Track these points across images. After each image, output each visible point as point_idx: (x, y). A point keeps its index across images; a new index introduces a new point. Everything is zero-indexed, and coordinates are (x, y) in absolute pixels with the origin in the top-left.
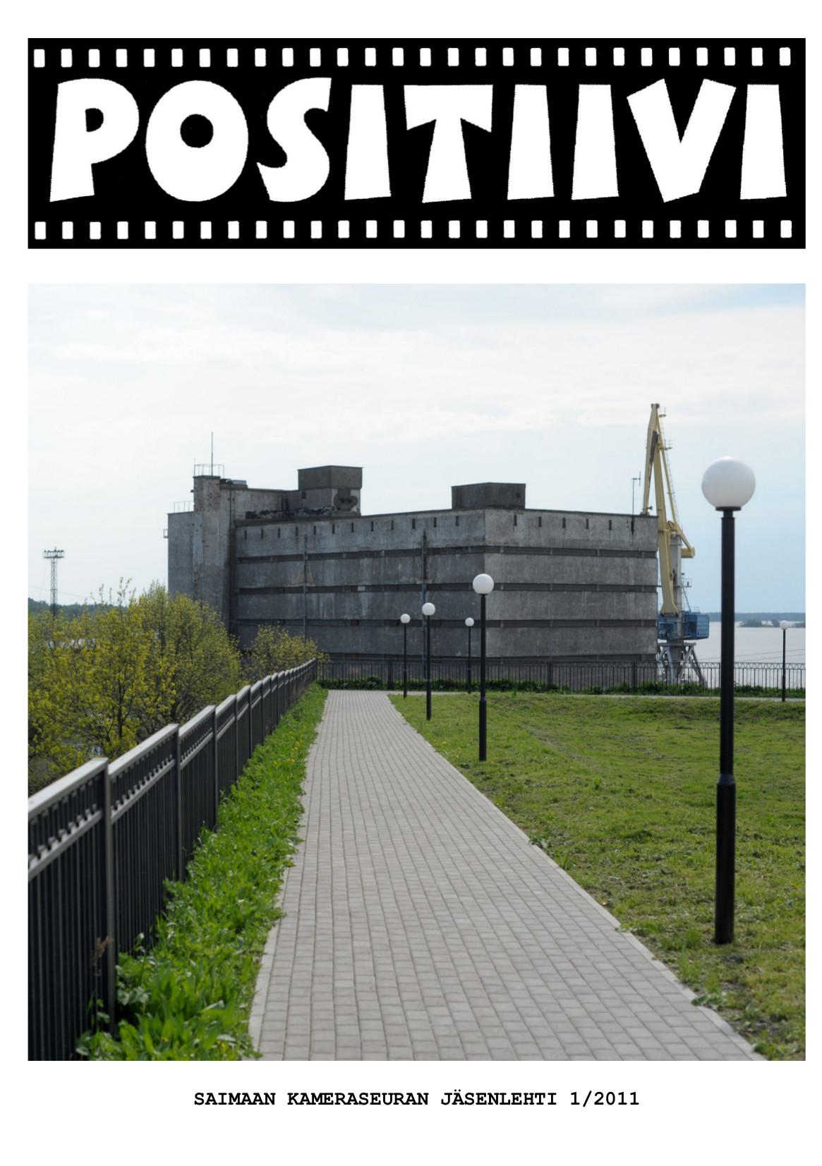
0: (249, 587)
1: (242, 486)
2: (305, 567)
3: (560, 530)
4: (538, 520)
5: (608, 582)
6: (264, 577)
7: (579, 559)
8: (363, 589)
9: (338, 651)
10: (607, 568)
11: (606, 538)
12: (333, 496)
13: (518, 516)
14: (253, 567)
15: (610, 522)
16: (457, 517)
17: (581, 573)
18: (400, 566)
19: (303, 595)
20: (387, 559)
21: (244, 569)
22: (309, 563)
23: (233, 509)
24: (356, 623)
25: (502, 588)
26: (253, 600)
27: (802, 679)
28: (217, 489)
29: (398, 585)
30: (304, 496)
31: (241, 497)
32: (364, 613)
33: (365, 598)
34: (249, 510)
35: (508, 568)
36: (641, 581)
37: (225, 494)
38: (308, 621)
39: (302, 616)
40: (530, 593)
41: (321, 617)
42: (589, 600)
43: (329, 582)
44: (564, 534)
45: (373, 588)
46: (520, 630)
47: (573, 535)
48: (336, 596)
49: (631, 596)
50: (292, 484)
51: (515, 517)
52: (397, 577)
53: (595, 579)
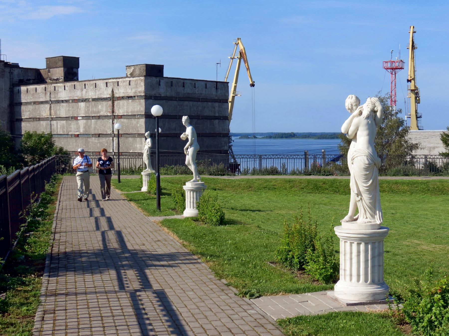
1: (16, 66)
3: (182, 88)
5: (205, 114)
6: (29, 113)
7: (191, 103)
13: (161, 80)
18: (100, 106)
22: (52, 105)
24: (78, 136)
31: (16, 72)
32: (82, 131)
33: (82, 123)
37: (7, 70)
40: (167, 119)
44: (184, 90)
45: (87, 118)
47: (188, 90)
48: (66, 122)
52: (99, 112)
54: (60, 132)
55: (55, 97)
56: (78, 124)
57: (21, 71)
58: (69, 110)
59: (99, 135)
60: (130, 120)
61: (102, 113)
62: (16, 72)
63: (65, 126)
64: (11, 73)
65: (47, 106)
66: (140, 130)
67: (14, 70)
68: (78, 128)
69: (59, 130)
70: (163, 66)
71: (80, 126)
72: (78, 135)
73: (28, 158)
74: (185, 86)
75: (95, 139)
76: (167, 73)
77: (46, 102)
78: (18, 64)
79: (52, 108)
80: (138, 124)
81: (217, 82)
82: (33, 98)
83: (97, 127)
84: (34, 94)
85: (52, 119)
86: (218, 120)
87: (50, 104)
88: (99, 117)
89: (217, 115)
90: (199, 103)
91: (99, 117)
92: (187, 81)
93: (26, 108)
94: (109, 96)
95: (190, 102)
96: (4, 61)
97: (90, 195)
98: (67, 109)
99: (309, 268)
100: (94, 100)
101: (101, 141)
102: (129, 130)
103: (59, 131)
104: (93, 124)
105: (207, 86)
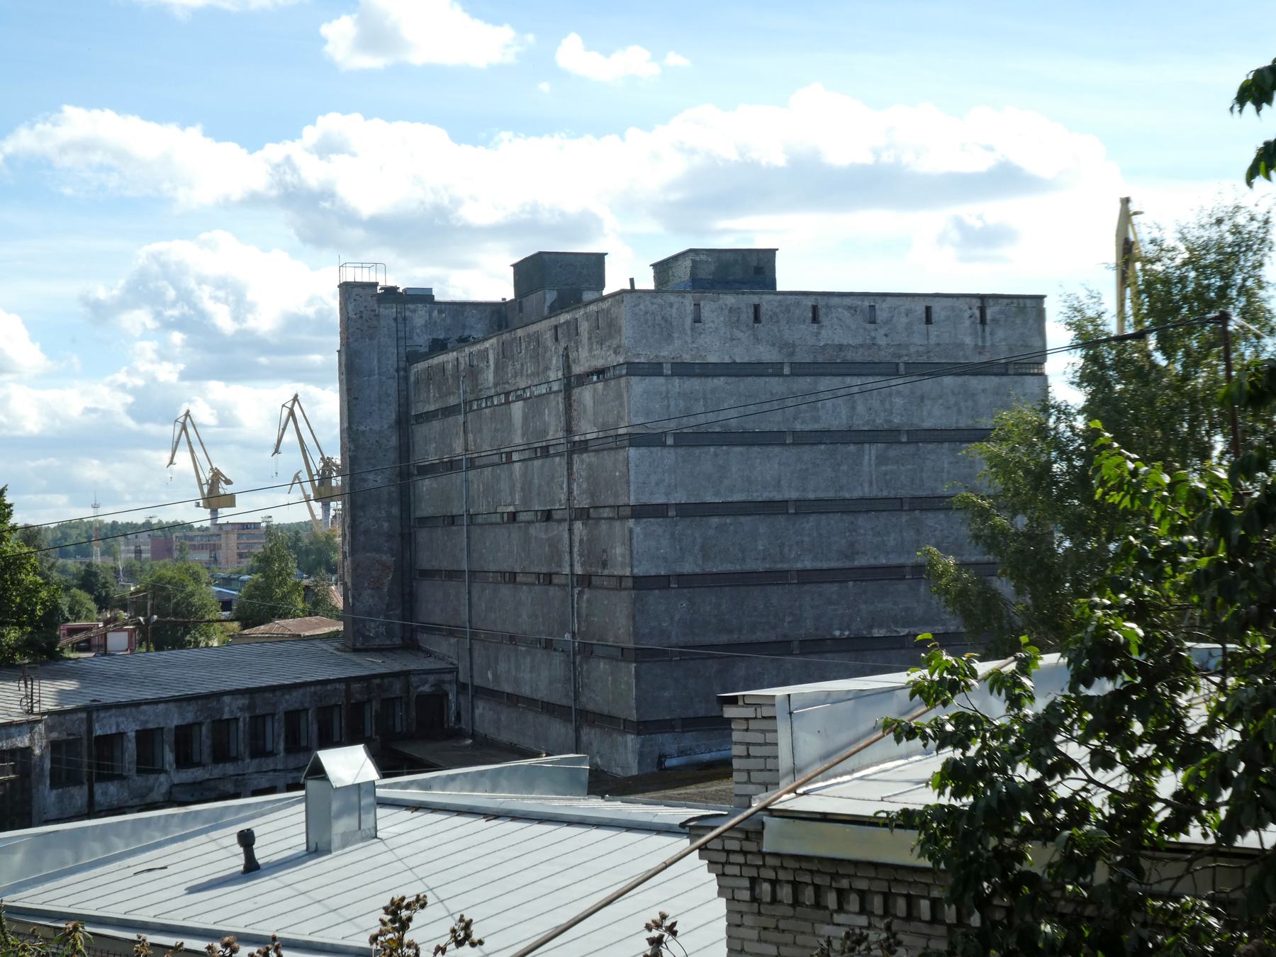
1: (423, 297)
5: (927, 424)
12: (548, 303)
13: (702, 303)
17: (861, 408)
25: (670, 441)
27: (347, 841)
34: (435, 336)
35: (682, 403)
36: (632, 297)
37: (389, 311)
42: (882, 460)
44: (818, 334)
46: (715, 521)
47: (834, 333)
51: (697, 305)
53: (897, 420)
57: (440, 312)
62: (419, 316)
67: (414, 311)
74: (825, 321)
76: (787, 279)
78: (431, 290)
81: (982, 298)
92: (836, 300)
97: (996, 902)
105: (935, 317)
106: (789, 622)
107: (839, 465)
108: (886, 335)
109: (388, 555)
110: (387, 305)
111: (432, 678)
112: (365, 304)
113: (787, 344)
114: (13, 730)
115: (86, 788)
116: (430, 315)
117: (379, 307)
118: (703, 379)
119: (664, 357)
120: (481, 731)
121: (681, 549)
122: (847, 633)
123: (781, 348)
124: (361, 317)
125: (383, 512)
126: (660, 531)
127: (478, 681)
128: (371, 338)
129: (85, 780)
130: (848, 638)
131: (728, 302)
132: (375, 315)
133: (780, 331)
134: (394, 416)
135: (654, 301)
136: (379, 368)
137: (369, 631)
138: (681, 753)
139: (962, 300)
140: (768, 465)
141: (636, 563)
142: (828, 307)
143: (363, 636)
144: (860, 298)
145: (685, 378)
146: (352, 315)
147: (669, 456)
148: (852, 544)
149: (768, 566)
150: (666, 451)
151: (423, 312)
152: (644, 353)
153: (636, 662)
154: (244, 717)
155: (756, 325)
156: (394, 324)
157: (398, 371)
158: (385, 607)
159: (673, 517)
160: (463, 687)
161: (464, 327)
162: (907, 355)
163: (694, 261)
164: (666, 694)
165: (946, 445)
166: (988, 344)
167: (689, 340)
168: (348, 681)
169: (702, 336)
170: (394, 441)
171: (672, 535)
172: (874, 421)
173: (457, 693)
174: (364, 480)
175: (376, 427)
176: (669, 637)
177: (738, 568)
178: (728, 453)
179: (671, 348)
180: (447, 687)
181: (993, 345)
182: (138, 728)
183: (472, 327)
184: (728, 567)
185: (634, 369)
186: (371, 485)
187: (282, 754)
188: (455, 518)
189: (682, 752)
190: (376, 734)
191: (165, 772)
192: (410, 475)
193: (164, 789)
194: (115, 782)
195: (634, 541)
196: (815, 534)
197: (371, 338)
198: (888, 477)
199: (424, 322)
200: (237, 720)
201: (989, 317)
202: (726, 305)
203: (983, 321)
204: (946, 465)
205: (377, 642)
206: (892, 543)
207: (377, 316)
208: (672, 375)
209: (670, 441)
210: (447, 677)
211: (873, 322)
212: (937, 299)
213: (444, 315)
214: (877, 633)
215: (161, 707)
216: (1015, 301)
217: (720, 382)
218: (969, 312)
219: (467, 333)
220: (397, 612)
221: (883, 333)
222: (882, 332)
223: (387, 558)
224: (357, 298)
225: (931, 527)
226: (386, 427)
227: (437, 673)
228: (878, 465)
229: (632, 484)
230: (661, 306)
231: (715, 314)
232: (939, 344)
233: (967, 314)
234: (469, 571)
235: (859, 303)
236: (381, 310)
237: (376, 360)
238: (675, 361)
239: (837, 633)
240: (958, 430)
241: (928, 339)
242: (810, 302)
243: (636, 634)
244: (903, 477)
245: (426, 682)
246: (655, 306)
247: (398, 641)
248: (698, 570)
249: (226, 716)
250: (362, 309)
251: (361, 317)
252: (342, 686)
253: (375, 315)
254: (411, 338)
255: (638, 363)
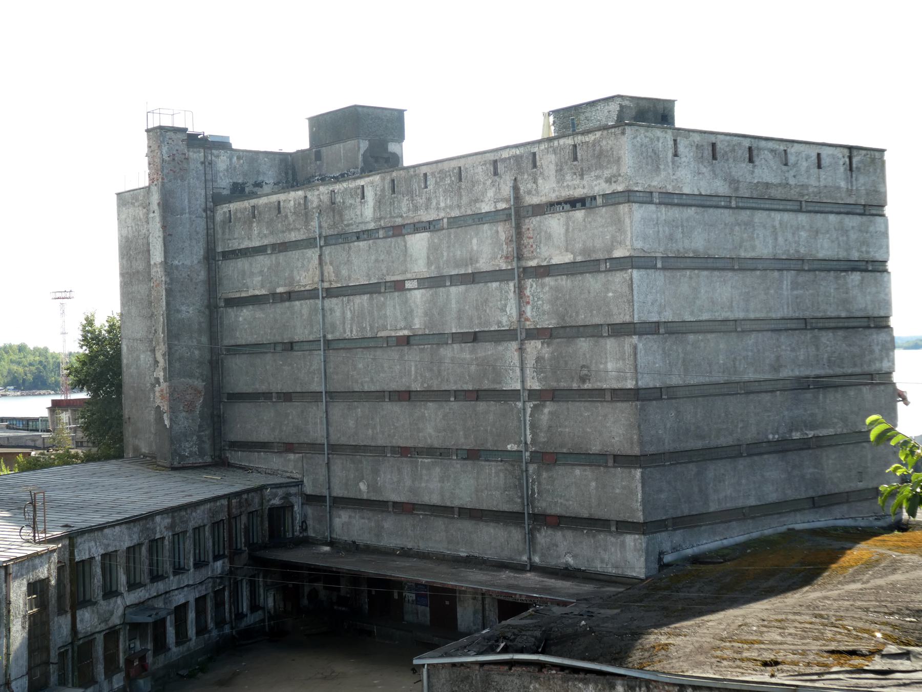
0: (238, 295)
1: (223, 145)
2: (320, 256)
3: (745, 166)
4: (710, 148)
5: (821, 255)
6: (260, 278)
8: (415, 284)
9: (378, 389)
10: (817, 232)
11: (813, 182)
12: (362, 151)
13: (679, 139)
14: (242, 264)
15: (819, 155)
16: (575, 146)
18: (475, 241)
19: (319, 302)
20: (452, 231)
21: (232, 269)
22: (327, 250)
23: (209, 177)
24: (406, 341)
26: (245, 314)
28: (183, 147)
29: (473, 274)
30: (318, 156)
32: (418, 324)
33: (418, 297)
35: (667, 229)
36: (868, 252)
37: (197, 156)
38: (328, 343)
39: (317, 334)
41: (348, 335)
43: (360, 279)
44: (753, 172)
45: (433, 282)
48: (371, 299)
49: (856, 277)
50: (303, 143)
52: (472, 260)
54: (351, 331)
55: (334, 225)
56: (406, 302)
57: (239, 158)
58: (377, 261)
59: (475, 337)
60: (579, 277)
61: (484, 265)
62: (222, 162)
63: (366, 311)
64: (208, 164)
65: (312, 255)
66: (615, 311)
67: (218, 156)
68: (409, 315)
69: (348, 327)
70: (672, 102)
71: (412, 311)
72: (408, 337)
73: (20, 458)
75: (462, 350)
76: (681, 121)
77: (309, 243)
79: (327, 258)
80: (608, 290)
82: (272, 233)
83: (467, 307)
84: (272, 220)
85: (330, 293)
86: (859, 273)
87: (321, 247)
88: (473, 278)
89: (855, 255)
90: (802, 218)
91: (473, 278)
92: (763, 144)
93: (251, 264)
94: (502, 206)
95: (773, 214)
96: (186, 129)
98: (373, 258)
99: (662, 496)
100: (454, 222)
101: (483, 354)
102: (577, 313)
103: (348, 330)
104: (453, 302)
105: (823, 162)
106: (741, 428)
107: (768, 289)
108: (794, 176)
109: (199, 380)
110: (195, 150)
111: (280, 492)
112: (177, 148)
113: (734, 180)
114: (37, 561)
115: (69, 616)
116: (231, 160)
117: (188, 151)
118: (681, 208)
119: (654, 186)
120: (346, 538)
121: (670, 363)
122: (777, 436)
123: (730, 184)
124: (174, 159)
125: (194, 340)
126: (655, 347)
127: (338, 492)
128: (183, 179)
129: (68, 609)
130: (778, 441)
131: (696, 140)
132: (185, 159)
133: (729, 168)
134: (202, 252)
135: (647, 134)
136: (189, 207)
137: (184, 450)
138: (674, 549)
139: (838, 149)
140: (724, 288)
141: (640, 376)
142: (759, 149)
143: (180, 455)
144: (778, 142)
145: (669, 206)
146: (166, 157)
147: (659, 278)
148: (778, 358)
149: (726, 378)
150: (658, 272)
151: (225, 157)
152: (641, 182)
153: (640, 467)
154: (168, 534)
155: (714, 161)
156: (201, 168)
157: (205, 210)
158: (197, 428)
159: (663, 334)
160: (310, 499)
161: (258, 173)
162: (807, 195)
163: (621, 106)
164: (662, 496)
165: (832, 273)
166: (854, 188)
167: (670, 171)
168: (228, 497)
169: (680, 169)
170: (203, 275)
171: (664, 349)
172: (789, 251)
173: (302, 504)
174: (178, 311)
175: (188, 263)
176: (664, 444)
177: (707, 380)
178: (699, 277)
179: (659, 179)
180: (293, 499)
181: (857, 190)
182: (103, 552)
183: (264, 174)
184: (702, 380)
185: (628, 196)
186: (184, 315)
187: (192, 570)
188: (294, 344)
189: (674, 549)
190: (245, 546)
191: (121, 594)
192: (217, 307)
193: (120, 611)
194: (89, 608)
195: (638, 356)
196: (755, 351)
197: (183, 179)
198: (798, 300)
199: (225, 167)
200: (163, 538)
201: (854, 166)
202: (694, 141)
203: (851, 169)
204: (832, 291)
205: (191, 460)
206: (802, 358)
207: (187, 159)
208: (660, 204)
209: (659, 265)
210: (293, 490)
211: (786, 164)
212: (824, 147)
213: (242, 161)
214: (796, 435)
215: (117, 528)
216: (869, 152)
217: (691, 211)
218: (843, 160)
219: (260, 179)
220: (207, 432)
221: (793, 174)
222: (792, 173)
223: (199, 384)
224: (170, 141)
225: (825, 343)
226: (196, 262)
227: (286, 487)
228: (792, 289)
229: (635, 304)
230: (651, 140)
231: (688, 149)
232: (826, 187)
233: (841, 163)
234: (326, 392)
235: (778, 147)
236: (191, 154)
237: (187, 200)
238: (661, 191)
239: (771, 437)
240: (581, 273)
241: (819, 181)
242: (746, 143)
243: (641, 443)
244: (807, 301)
245: (275, 495)
246: (648, 139)
247: (208, 459)
248: (681, 382)
249: (158, 536)
250: (175, 152)
251: (174, 159)
252: (225, 502)
253: (185, 159)
254: (216, 181)
255: (637, 191)
